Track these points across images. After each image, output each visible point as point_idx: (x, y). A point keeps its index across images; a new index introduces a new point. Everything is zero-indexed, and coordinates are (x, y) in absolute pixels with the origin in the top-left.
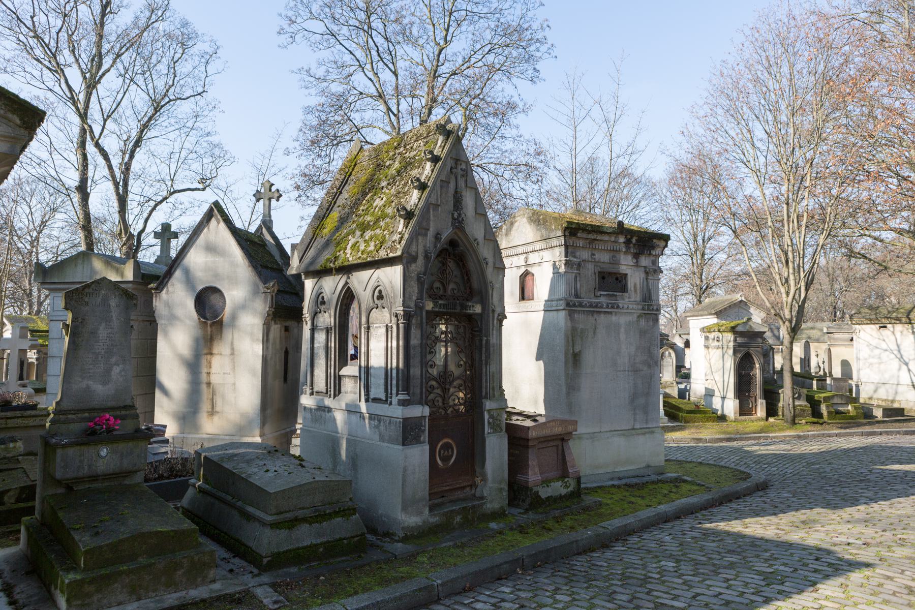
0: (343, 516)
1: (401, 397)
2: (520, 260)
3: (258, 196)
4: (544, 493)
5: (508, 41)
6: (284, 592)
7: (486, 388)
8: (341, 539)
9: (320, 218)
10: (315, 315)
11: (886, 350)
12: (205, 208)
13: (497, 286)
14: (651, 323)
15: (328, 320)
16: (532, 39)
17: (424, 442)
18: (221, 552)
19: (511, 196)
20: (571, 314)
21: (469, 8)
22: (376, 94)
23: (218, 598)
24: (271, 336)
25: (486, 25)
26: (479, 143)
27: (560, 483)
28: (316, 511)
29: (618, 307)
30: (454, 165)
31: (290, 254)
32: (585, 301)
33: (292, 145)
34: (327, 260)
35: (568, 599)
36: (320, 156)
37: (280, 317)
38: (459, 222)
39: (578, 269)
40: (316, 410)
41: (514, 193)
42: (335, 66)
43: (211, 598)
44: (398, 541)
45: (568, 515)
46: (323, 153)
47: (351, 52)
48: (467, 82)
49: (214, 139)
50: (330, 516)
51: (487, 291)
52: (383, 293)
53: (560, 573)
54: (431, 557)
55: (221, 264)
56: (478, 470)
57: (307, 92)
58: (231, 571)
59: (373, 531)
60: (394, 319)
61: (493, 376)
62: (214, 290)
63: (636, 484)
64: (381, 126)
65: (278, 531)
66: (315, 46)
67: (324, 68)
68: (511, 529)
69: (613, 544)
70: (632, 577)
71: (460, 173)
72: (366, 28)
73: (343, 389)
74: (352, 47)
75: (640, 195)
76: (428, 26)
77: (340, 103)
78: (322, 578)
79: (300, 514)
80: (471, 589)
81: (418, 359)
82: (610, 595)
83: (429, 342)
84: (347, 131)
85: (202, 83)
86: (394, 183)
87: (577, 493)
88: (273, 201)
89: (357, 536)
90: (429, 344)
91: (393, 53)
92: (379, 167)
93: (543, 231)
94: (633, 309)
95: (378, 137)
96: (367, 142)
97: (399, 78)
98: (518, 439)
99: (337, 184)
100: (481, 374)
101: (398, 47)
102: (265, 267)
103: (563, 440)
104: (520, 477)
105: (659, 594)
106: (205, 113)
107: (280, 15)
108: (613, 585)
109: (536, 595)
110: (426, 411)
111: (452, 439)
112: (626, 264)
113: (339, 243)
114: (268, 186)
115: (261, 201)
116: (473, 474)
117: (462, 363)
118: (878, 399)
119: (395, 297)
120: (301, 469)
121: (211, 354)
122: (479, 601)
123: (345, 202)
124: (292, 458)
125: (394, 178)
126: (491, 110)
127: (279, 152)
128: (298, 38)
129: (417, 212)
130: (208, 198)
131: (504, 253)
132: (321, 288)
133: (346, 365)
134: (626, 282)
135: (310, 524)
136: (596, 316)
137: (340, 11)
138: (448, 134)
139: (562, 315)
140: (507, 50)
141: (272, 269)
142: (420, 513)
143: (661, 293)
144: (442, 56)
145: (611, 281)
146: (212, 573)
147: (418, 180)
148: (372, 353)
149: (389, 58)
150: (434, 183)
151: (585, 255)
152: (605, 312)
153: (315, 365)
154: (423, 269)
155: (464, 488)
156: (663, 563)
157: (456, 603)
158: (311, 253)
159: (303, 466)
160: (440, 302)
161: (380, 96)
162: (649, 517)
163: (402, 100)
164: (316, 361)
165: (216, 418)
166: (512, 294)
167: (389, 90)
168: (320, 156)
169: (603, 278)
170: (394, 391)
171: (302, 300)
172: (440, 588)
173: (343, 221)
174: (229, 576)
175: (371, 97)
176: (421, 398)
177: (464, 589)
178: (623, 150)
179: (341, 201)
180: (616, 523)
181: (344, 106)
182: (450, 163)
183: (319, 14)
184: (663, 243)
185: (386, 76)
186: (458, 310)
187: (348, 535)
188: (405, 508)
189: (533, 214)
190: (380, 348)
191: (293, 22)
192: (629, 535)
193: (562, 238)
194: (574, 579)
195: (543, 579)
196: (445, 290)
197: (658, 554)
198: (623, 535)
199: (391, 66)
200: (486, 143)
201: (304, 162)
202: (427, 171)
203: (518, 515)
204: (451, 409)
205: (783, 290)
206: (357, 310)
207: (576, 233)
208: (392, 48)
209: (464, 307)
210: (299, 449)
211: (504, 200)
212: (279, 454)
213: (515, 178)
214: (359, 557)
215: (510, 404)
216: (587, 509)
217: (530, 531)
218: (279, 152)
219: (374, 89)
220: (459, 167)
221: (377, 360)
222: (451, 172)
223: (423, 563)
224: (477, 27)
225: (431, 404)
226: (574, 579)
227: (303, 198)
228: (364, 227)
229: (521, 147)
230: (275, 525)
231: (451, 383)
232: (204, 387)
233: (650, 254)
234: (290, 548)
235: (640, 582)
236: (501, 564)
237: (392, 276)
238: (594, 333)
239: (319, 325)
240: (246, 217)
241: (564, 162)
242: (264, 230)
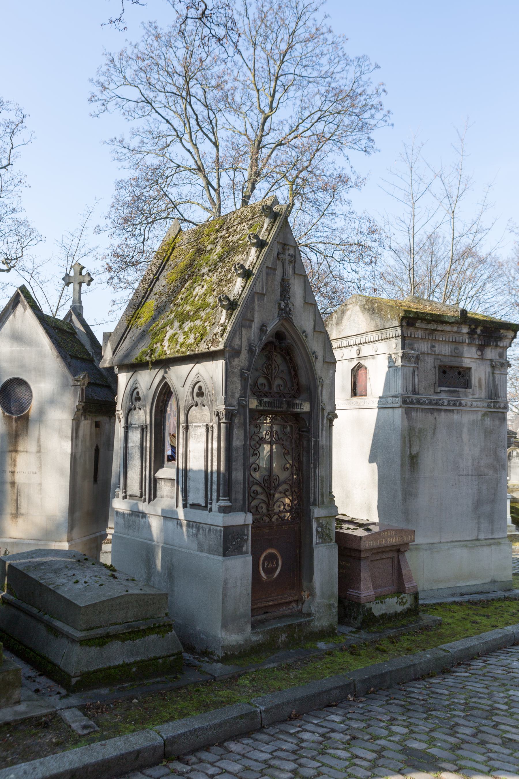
0: (158, 633)
1: (222, 503)
2: (352, 353)
3: (67, 280)
4: (378, 610)
5: (340, 108)
6: (94, 716)
7: (315, 494)
8: (156, 658)
9: (136, 306)
10: (129, 411)
12: (11, 292)
13: (327, 382)
14: (497, 422)
15: (143, 418)
16: (366, 105)
17: (246, 553)
18: (27, 670)
19: (341, 278)
20: (408, 412)
21: (297, 72)
22: (194, 166)
23: (23, 721)
24: (81, 433)
25: (316, 90)
26: (307, 221)
27: (395, 599)
28: (129, 627)
29: (460, 404)
30: (281, 251)
31: (101, 342)
32: (424, 398)
33: (103, 222)
34: (143, 353)
35: (405, 731)
36: (133, 235)
37: (90, 412)
38: (286, 313)
39: (416, 362)
40: (129, 515)
41: (345, 275)
42: (150, 136)
43: (16, 721)
44: (218, 661)
45: (404, 634)
46: (137, 232)
47: (168, 121)
48: (294, 153)
49: (20, 216)
50: (144, 633)
51: (316, 388)
52: (203, 390)
53: (396, 701)
54: (254, 679)
55: (28, 354)
56: (305, 584)
57: (120, 164)
58: (37, 691)
59: (190, 649)
61: (322, 481)
62: (20, 382)
63: (480, 601)
64: (200, 202)
65: (88, 648)
66: (128, 114)
67: (138, 139)
68: (341, 650)
69: (455, 669)
70: (477, 708)
71: (287, 258)
72: (184, 94)
73: (158, 494)
74: (170, 115)
75: (485, 276)
76: (252, 92)
77: (156, 177)
78: (135, 701)
79: (112, 630)
80: (297, 717)
81: (241, 462)
82: (452, 728)
83: (253, 443)
84: (163, 207)
85: (7, 155)
86: (216, 269)
87: (414, 612)
88: (84, 285)
89: (173, 655)
90: (252, 446)
91: (214, 122)
92: (200, 251)
93: (378, 321)
94: (477, 407)
95: (199, 215)
96: (185, 220)
97: (220, 149)
98: (349, 551)
99: (154, 269)
100: (309, 479)
101: (218, 115)
102: (73, 357)
103: (399, 551)
104: (351, 592)
105: (508, 728)
106: (11, 188)
107: (92, 80)
108: (455, 716)
109: (369, 726)
110: (249, 519)
111: (277, 548)
112: (469, 357)
113: (155, 335)
114: (78, 268)
115: (71, 285)
116: (300, 588)
117: (288, 466)
119: (216, 394)
120: (113, 580)
121: (16, 451)
122: (306, 731)
123: (163, 289)
124: (103, 568)
125: (216, 265)
126: (321, 184)
127: (90, 231)
128: (111, 105)
129: (240, 303)
130: (13, 281)
131: (334, 344)
132: (136, 382)
133: (162, 466)
134: (470, 377)
135: (123, 641)
136: (436, 414)
137: (157, 76)
138: (275, 216)
139: (398, 413)
140: (339, 117)
141: (82, 360)
142: (241, 631)
143: (509, 385)
144: (267, 124)
145: (454, 376)
146: (17, 694)
147: (242, 267)
148: (191, 455)
149: (210, 127)
150: (260, 271)
151: (424, 347)
152: (446, 410)
153: (129, 466)
154: (247, 364)
155: (290, 603)
156: (511, 693)
157: (281, 732)
158: (126, 345)
159: (115, 577)
160: (265, 400)
161: (199, 169)
162: (495, 640)
163: (223, 174)
164: (130, 462)
165: (20, 521)
166: (343, 389)
167: (209, 163)
168: (133, 235)
169: (444, 372)
170: (215, 497)
171: (114, 392)
172: (263, 715)
173: (160, 310)
174: (35, 696)
175: (190, 170)
176: (244, 504)
177: (290, 717)
178: (466, 229)
179: (158, 288)
180: (459, 645)
181: (160, 181)
182: (277, 248)
183: (134, 80)
184: (511, 334)
185: (206, 147)
186: (284, 408)
187: (164, 654)
188: (224, 626)
189: (367, 302)
190: (199, 449)
191: (105, 88)
192: (473, 659)
193: (399, 329)
194: (411, 707)
195: (376, 707)
196: (270, 388)
197: (505, 682)
198: (466, 659)
199: (211, 136)
200: (315, 221)
201: (116, 241)
202: (251, 257)
203: (349, 635)
204: (276, 517)
206: (174, 408)
207: (416, 324)
208: (212, 116)
209: (291, 405)
210: (110, 556)
211: (334, 283)
212: (89, 564)
213: (346, 259)
214: (176, 678)
215: (340, 511)
216: (426, 628)
217: (362, 652)
218: (90, 231)
219: (193, 161)
220: (287, 253)
221: (196, 462)
222: (278, 258)
223: (245, 686)
224: (306, 93)
225: (255, 511)
226: (411, 707)
227: (115, 281)
228: (183, 318)
229: (353, 225)
230: (85, 642)
231: (276, 488)
232: (8, 487)
233: (497, 346)
234: (101, 666)
235: (485, 714)
236: (331, 690)
237: (214, 372)
238: (434, 433)
239: (133, 423)
240: (54, 301)
241: (401, 240)
242: (74, 317)
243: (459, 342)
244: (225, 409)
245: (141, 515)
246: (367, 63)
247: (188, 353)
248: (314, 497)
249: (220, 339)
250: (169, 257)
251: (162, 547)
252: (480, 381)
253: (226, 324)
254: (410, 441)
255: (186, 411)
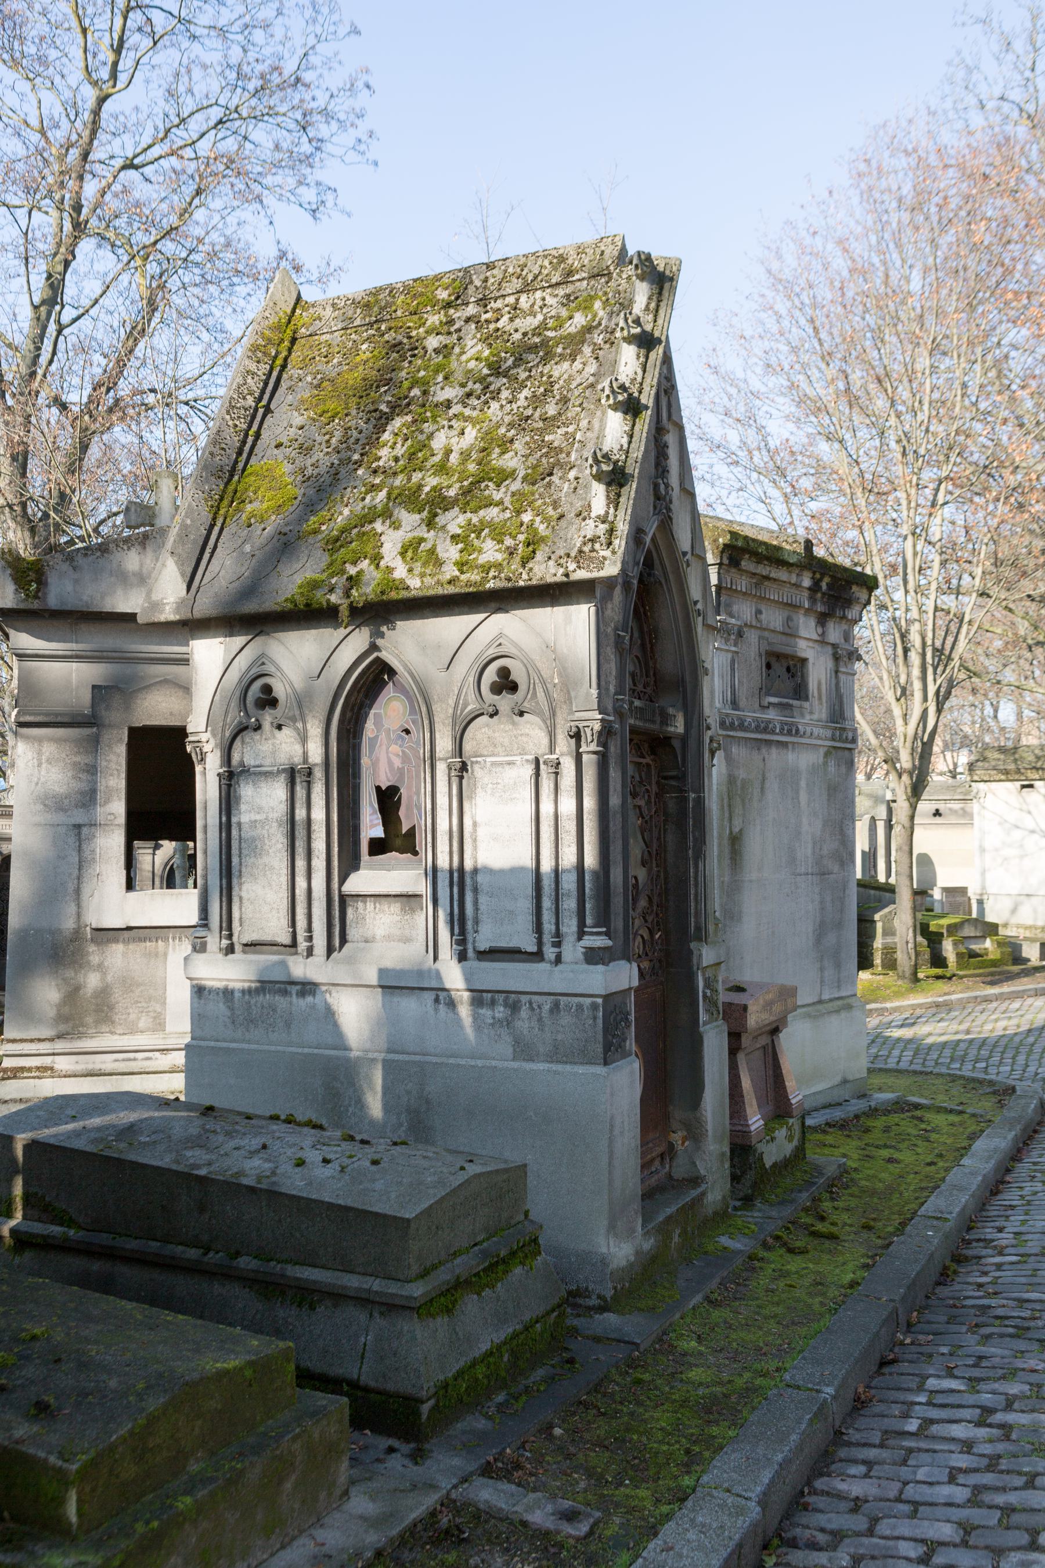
1: (589, 941)
11: (1033, 832)
40: (248, 992)
44: (603, 1309)
60: (564, 745)
73: (352, 933)
89: (553, 1310)
99: (254, 384)
118: (1018, 926)
170: (570, 926)
184: (863, 595)
205: (897, 712)
233: (844, 617)
234: (462, 1363)
238: (762, 788)
243: (795, 606)
244: (602, 720)
245: (294, 989)
246: (335, 17)
247: (491, 585)
248: (696, 922)
249: (607, 553)
250: (286, 359)
251: (384, 1061)
252: (819, 684)
253: (611, 518)
254: (730, 806)
255: (459, 729)
